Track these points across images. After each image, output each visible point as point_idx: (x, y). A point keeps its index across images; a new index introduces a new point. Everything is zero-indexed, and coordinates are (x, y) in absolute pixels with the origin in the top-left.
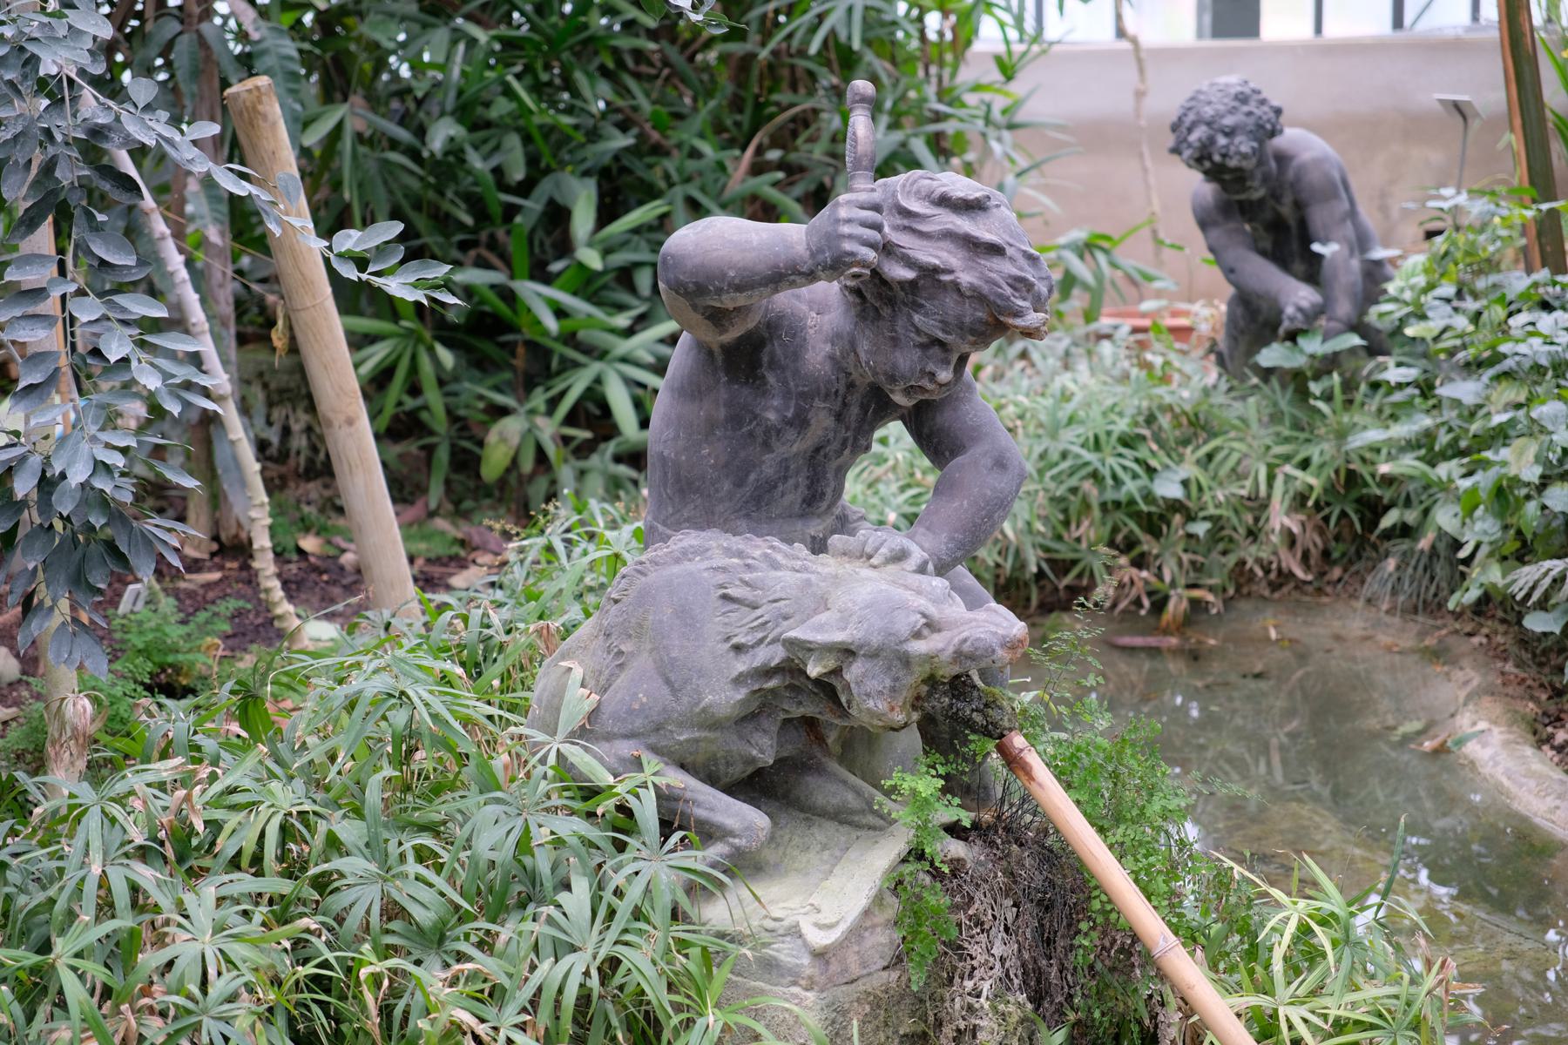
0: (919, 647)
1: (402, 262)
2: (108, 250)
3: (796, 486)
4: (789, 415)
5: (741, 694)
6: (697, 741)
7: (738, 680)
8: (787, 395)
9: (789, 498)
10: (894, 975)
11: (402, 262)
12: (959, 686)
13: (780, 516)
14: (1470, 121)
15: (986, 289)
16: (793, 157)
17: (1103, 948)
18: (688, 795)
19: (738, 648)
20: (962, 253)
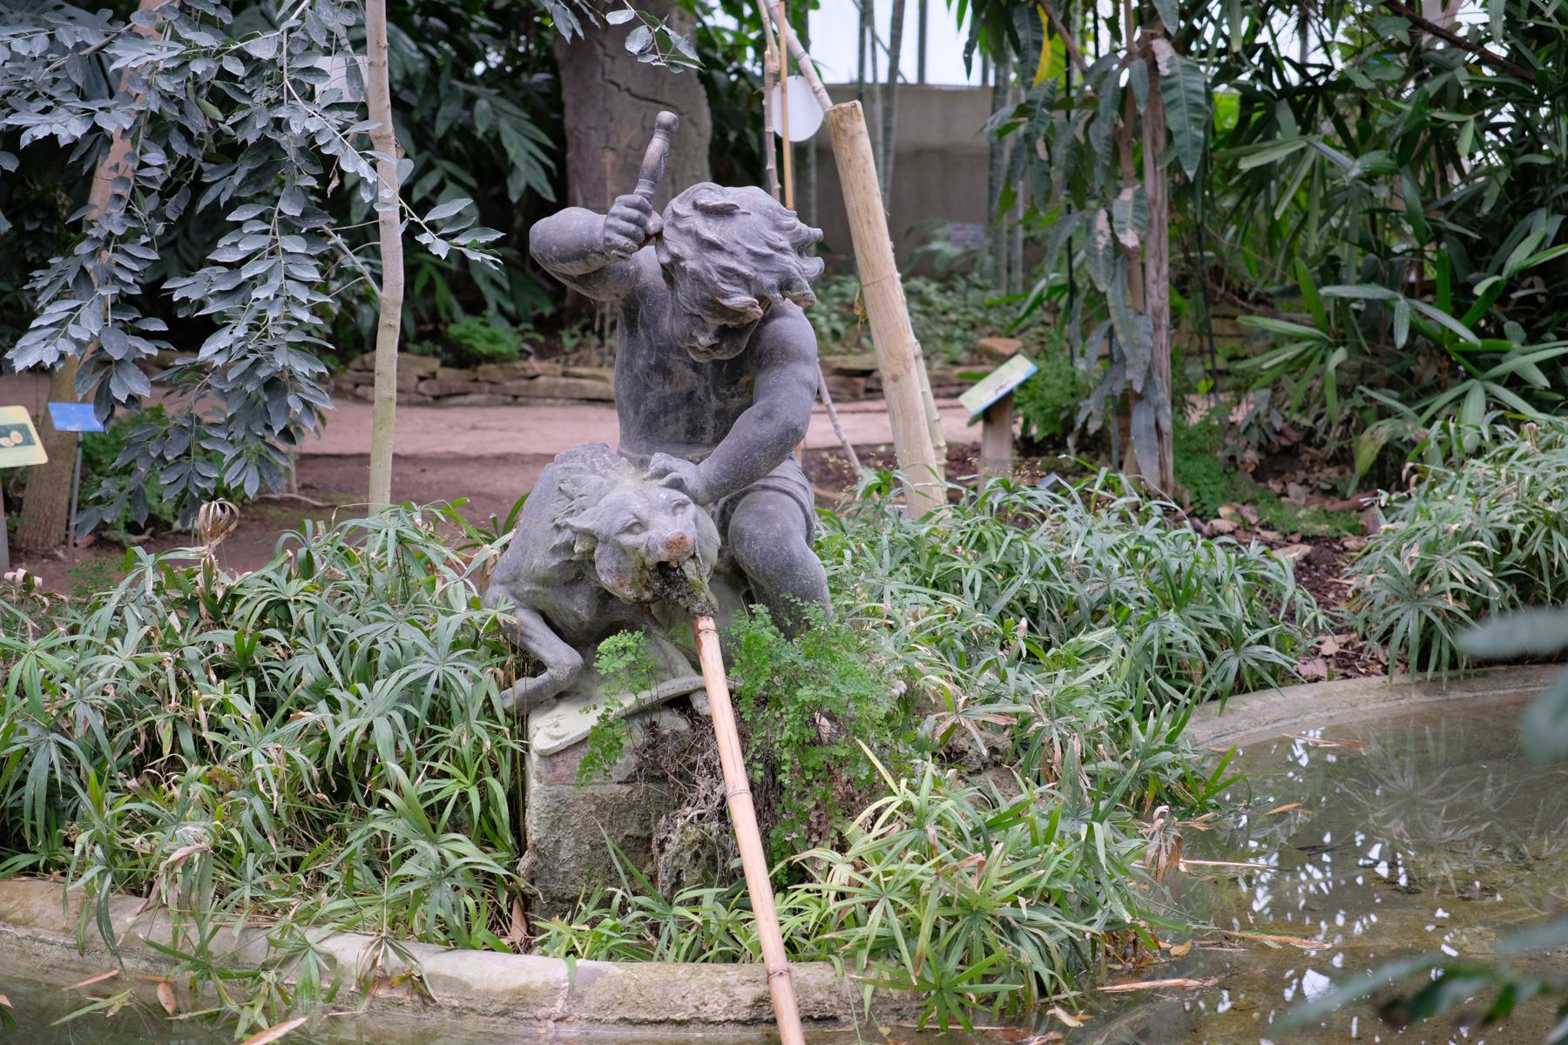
0: (628, 539)
1: (473, 226)
2: (917, 415)
3: (677, 420)
4: (652, 362)
5: (555, 562)
6: (536, 593)
7: (555, 551)
8: (651, 348)
9: (672, 428)
10: (626, 789)
11: (473, 226)
12: (663, 567)
13: (668, 441)
14: (1153, 424)
15: (703, 274)
16: (843, 290)
17: (1179, 586)
18: (528, 632)
19: (558, 528)
20: (695, 247)
